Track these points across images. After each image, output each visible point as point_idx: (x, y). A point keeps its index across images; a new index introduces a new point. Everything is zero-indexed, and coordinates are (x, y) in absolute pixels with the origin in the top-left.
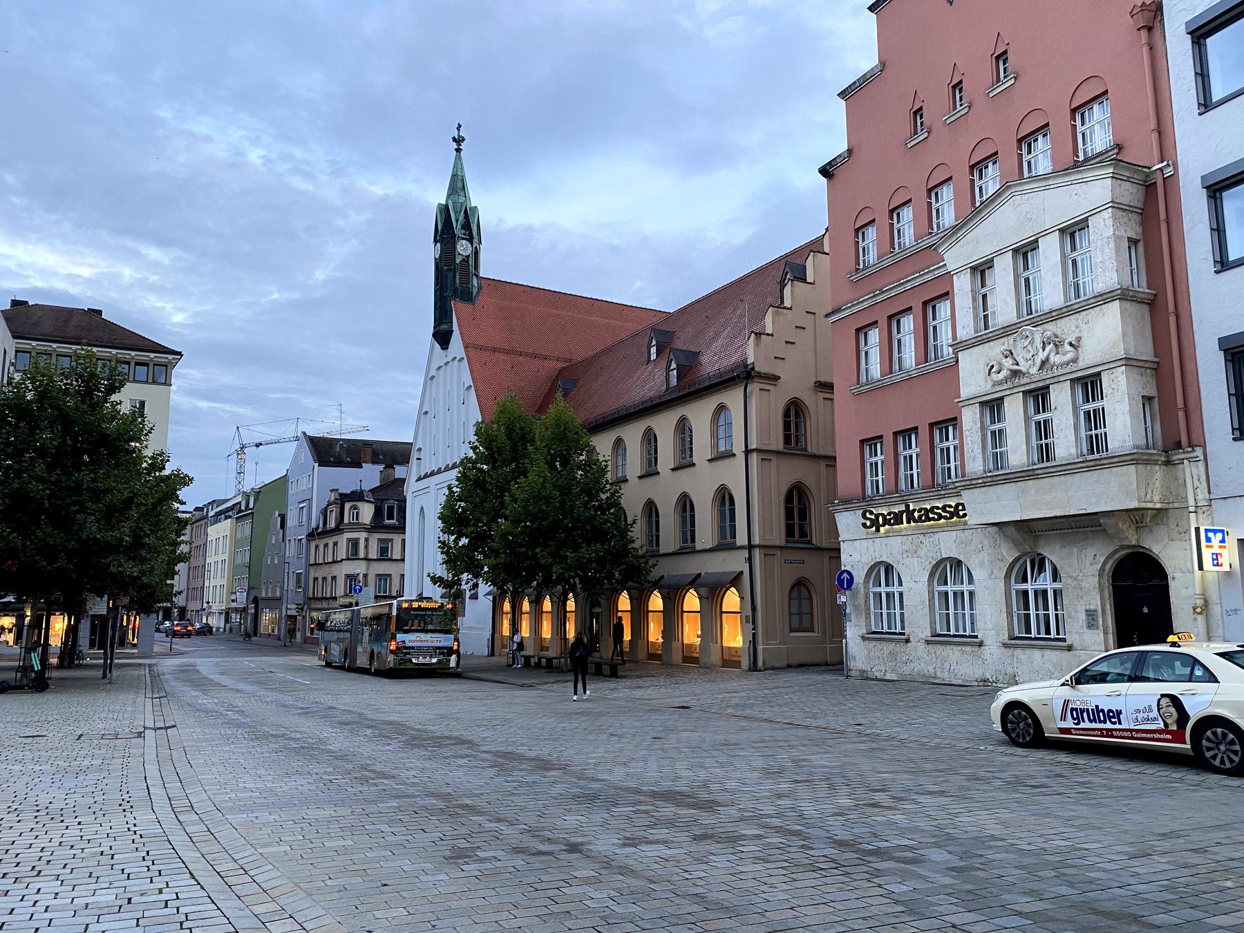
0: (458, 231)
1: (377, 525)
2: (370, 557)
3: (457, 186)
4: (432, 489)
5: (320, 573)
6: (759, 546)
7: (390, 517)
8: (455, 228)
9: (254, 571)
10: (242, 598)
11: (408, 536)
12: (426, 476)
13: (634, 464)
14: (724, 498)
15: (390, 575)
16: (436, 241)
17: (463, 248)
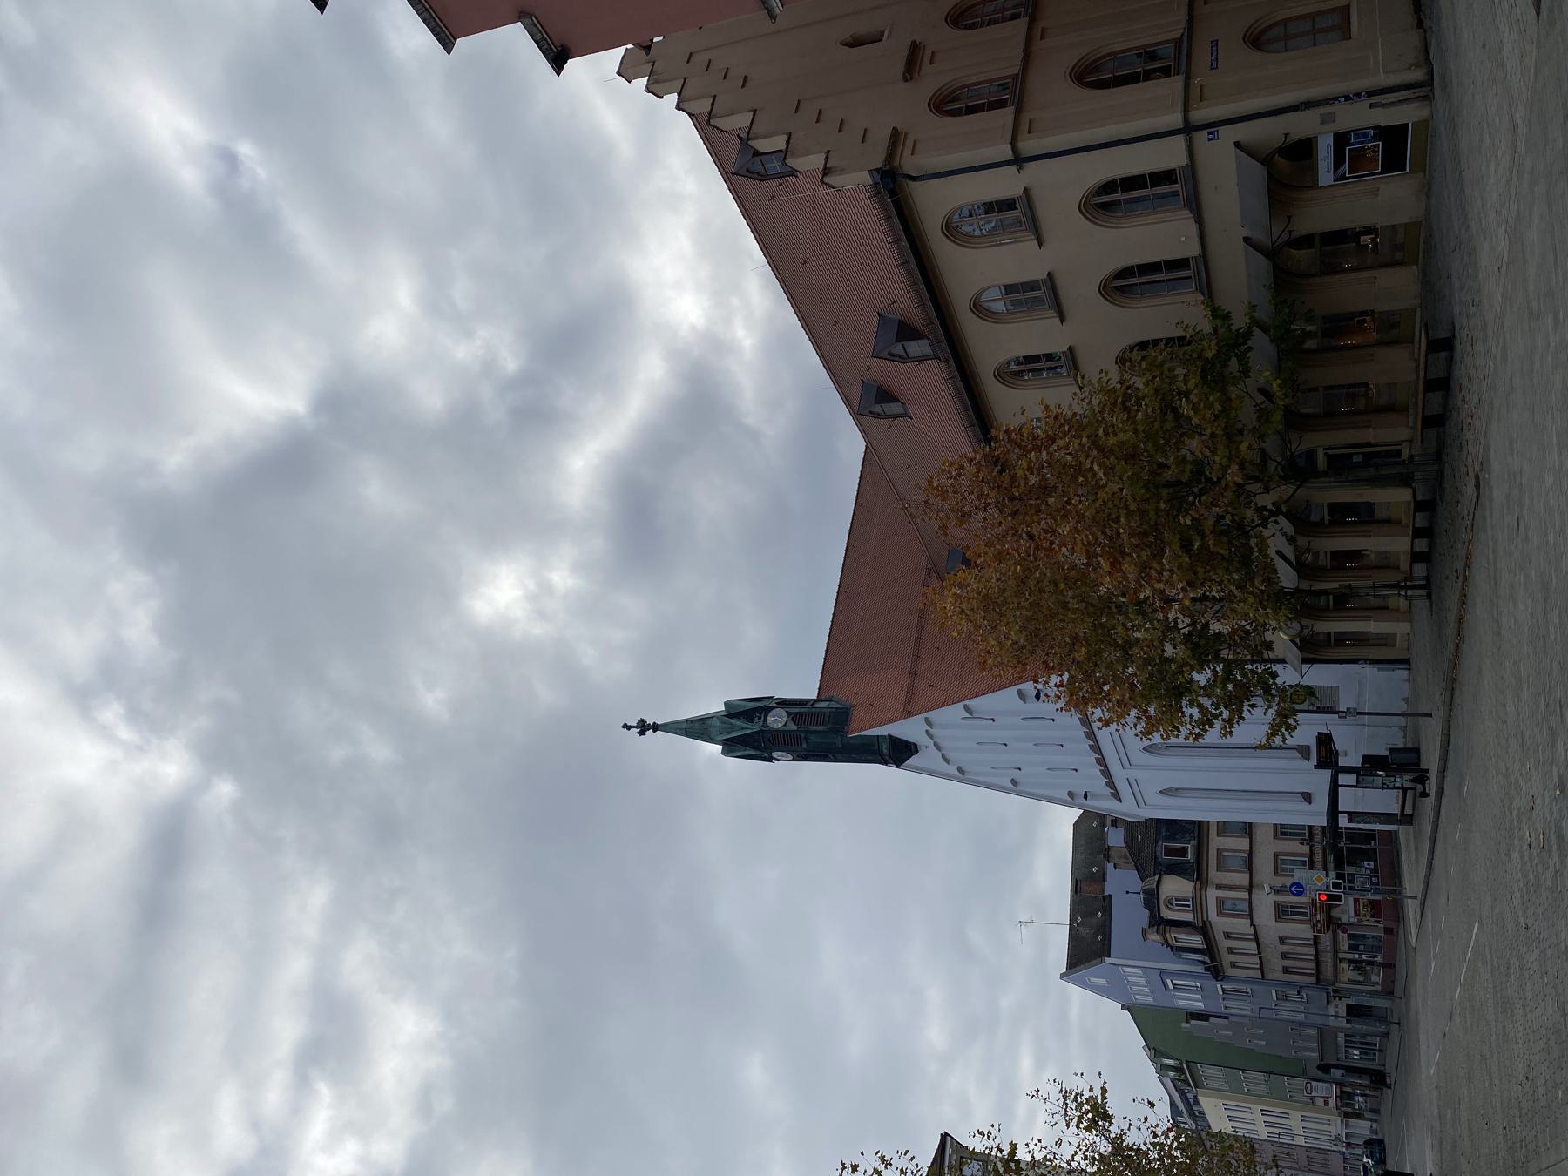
0: (750, 728)
1: (1196, 872)
2: (1246, 883)
3: (697, 728)
4: (1133, 774)
5: (1275, 964)
6: (1186, 111)
7: (1183, 852)
8: (752, 730)
9: (1274, 1069)
10: (1325, 1090)
11: (1213, 817)
12: (1111, 784)
13: (1061, 396)
14: (1106, 201)
15: (1276, 855)
16: (771, 759)
17: (777, 720)
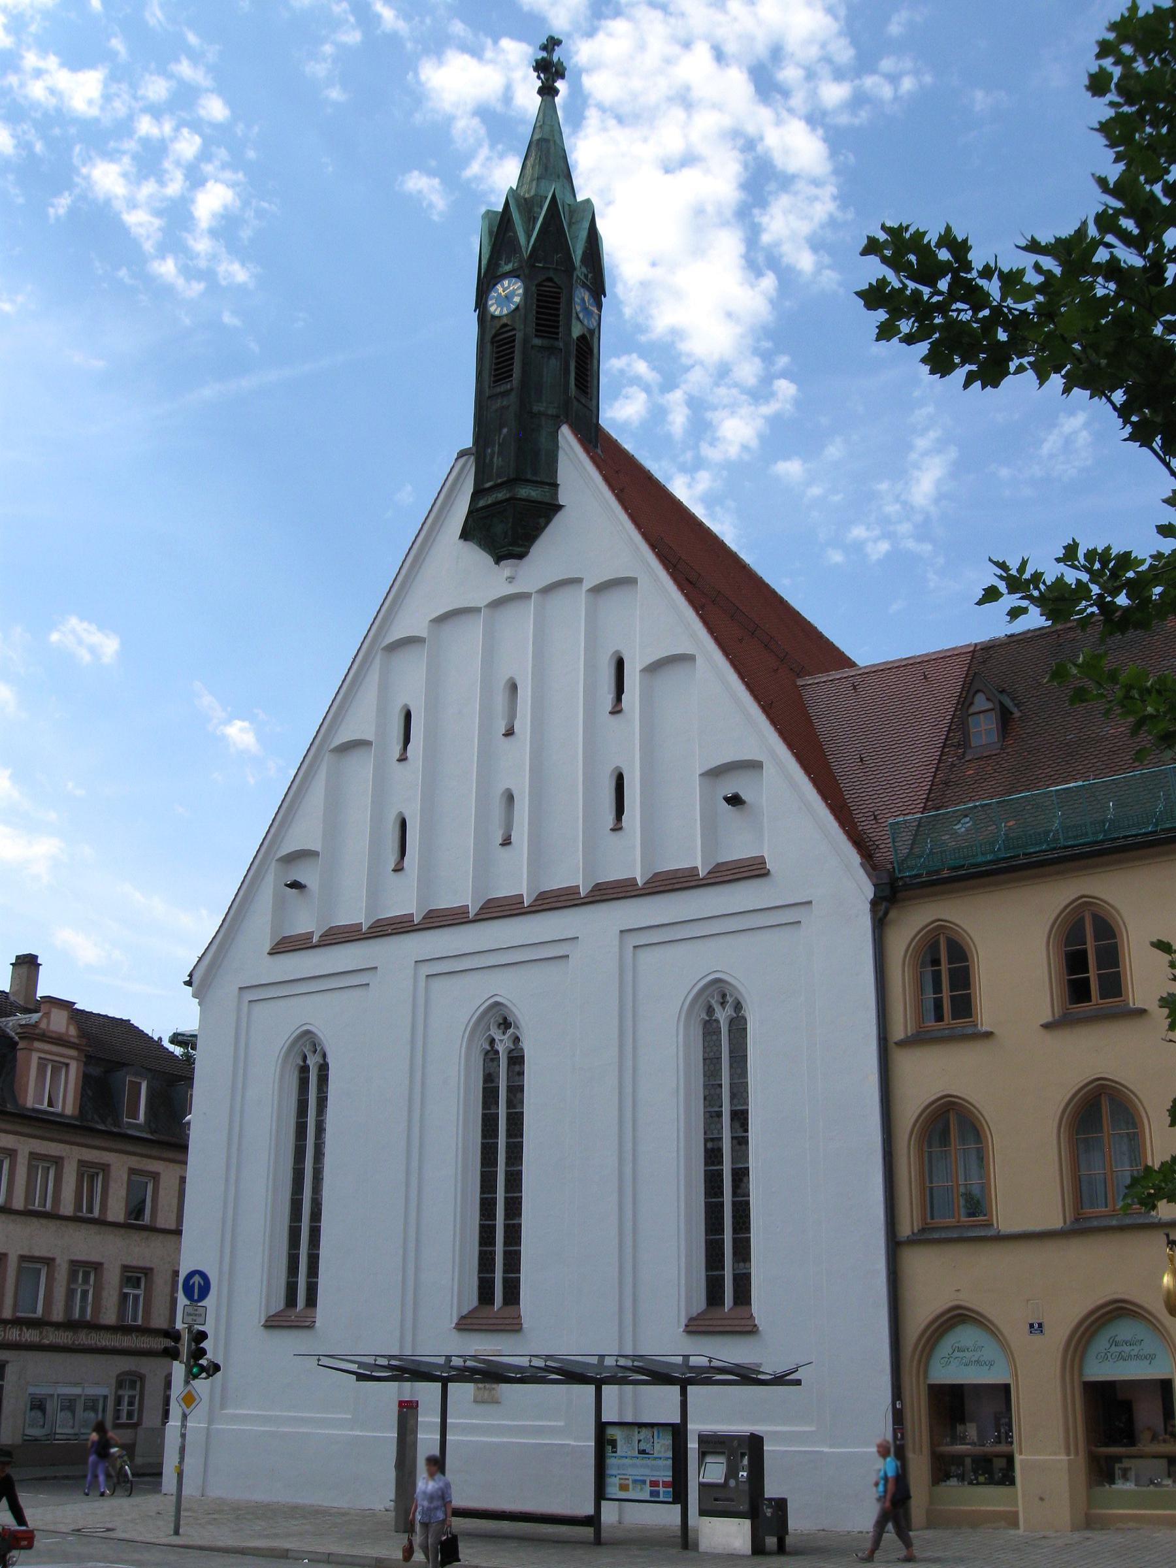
3: (547, 154)
